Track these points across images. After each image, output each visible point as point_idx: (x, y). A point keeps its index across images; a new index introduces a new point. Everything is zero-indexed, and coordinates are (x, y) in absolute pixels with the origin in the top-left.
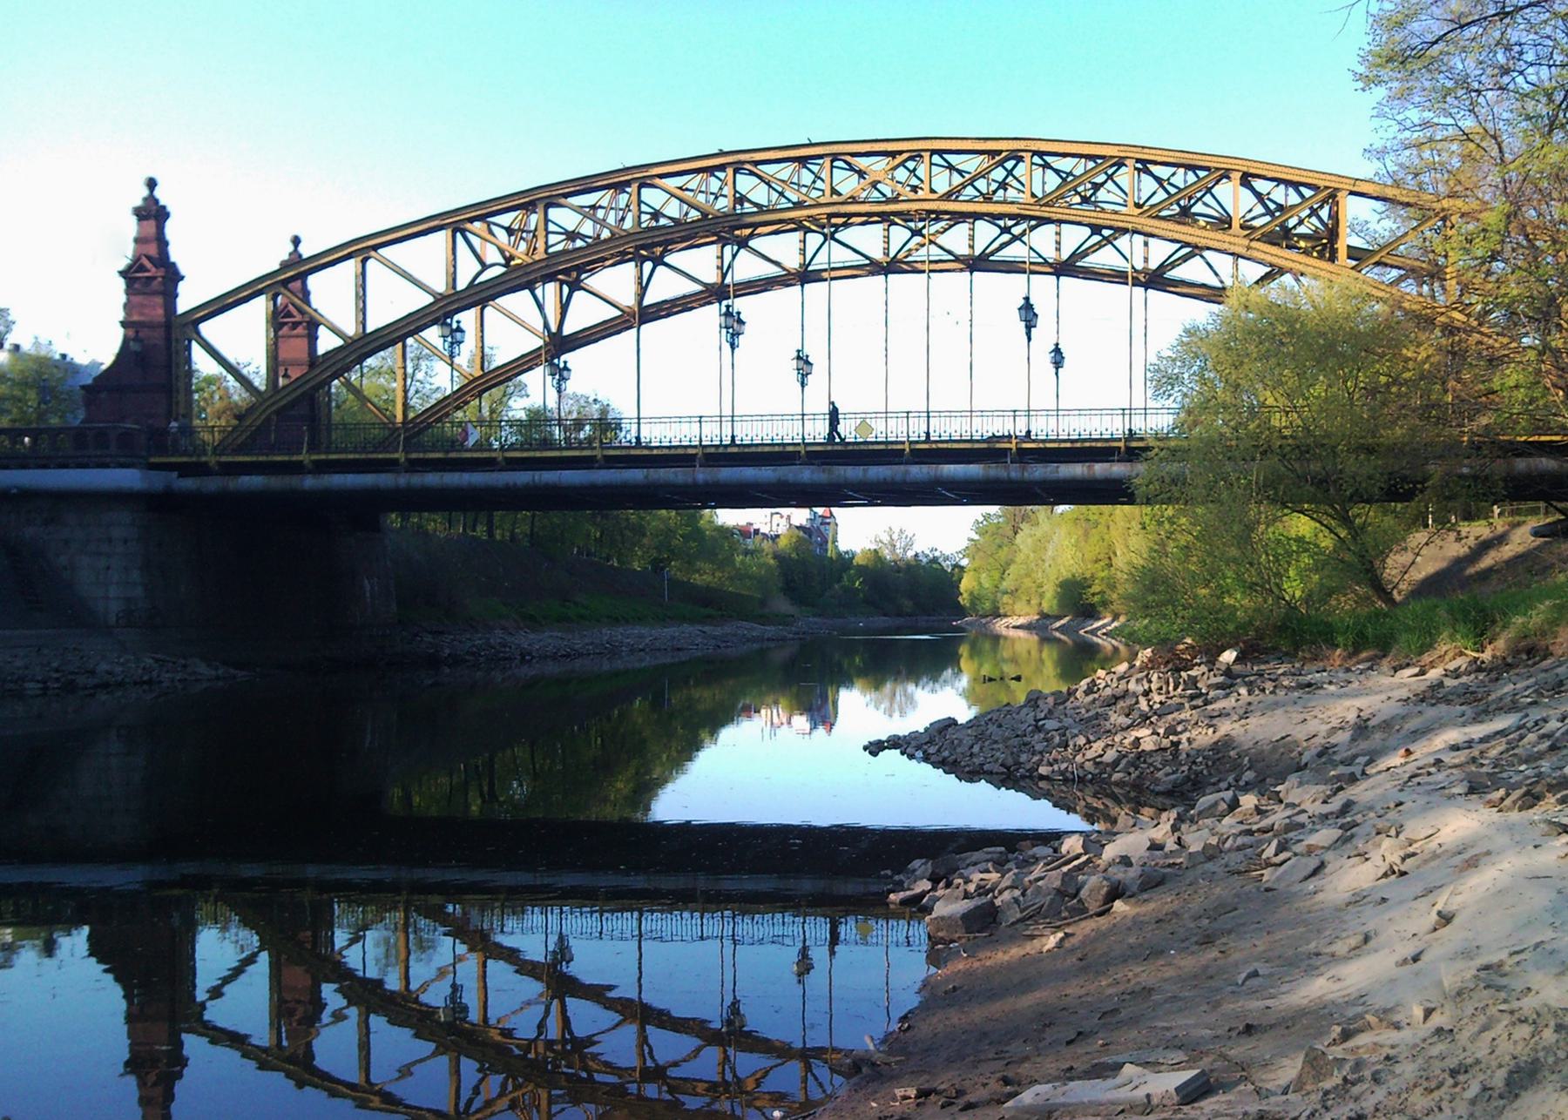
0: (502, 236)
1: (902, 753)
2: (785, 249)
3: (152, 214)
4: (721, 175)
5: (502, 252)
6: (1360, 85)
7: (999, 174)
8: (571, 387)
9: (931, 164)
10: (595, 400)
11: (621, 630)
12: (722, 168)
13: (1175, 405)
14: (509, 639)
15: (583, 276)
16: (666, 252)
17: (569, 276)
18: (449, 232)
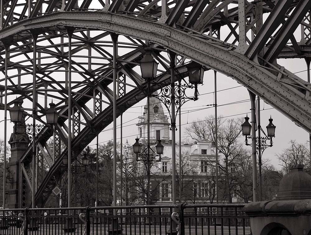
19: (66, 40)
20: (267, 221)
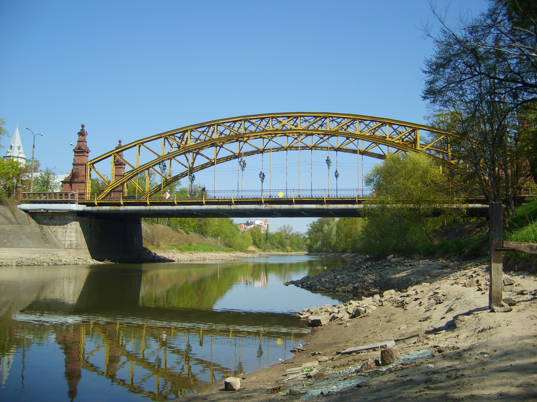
0: (177, 139)
1: (295, 285)
2: (259, 143)
3: (82, 134)
4: (240, 122)
5: (177, 144)
6: (423, 99)
7: (320, 123)
8: (195, 182)
9: (300, 120)
10: (200, 187)
11: (206, 254)
12: (240, 120)
13: (371, 188)
14: (175, 255)
15: (200, 151)
16: (224, 143)
17: (196, 151)
18: (163, 139)
20: (315, 219)
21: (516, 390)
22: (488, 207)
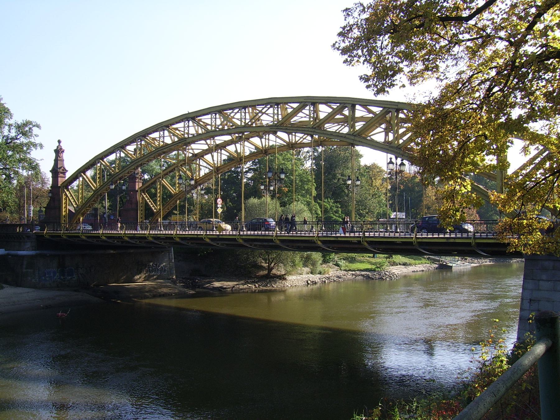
19: (458, 187)
20: (68, 175)
21: (536, 353)
22: (307, 121)
